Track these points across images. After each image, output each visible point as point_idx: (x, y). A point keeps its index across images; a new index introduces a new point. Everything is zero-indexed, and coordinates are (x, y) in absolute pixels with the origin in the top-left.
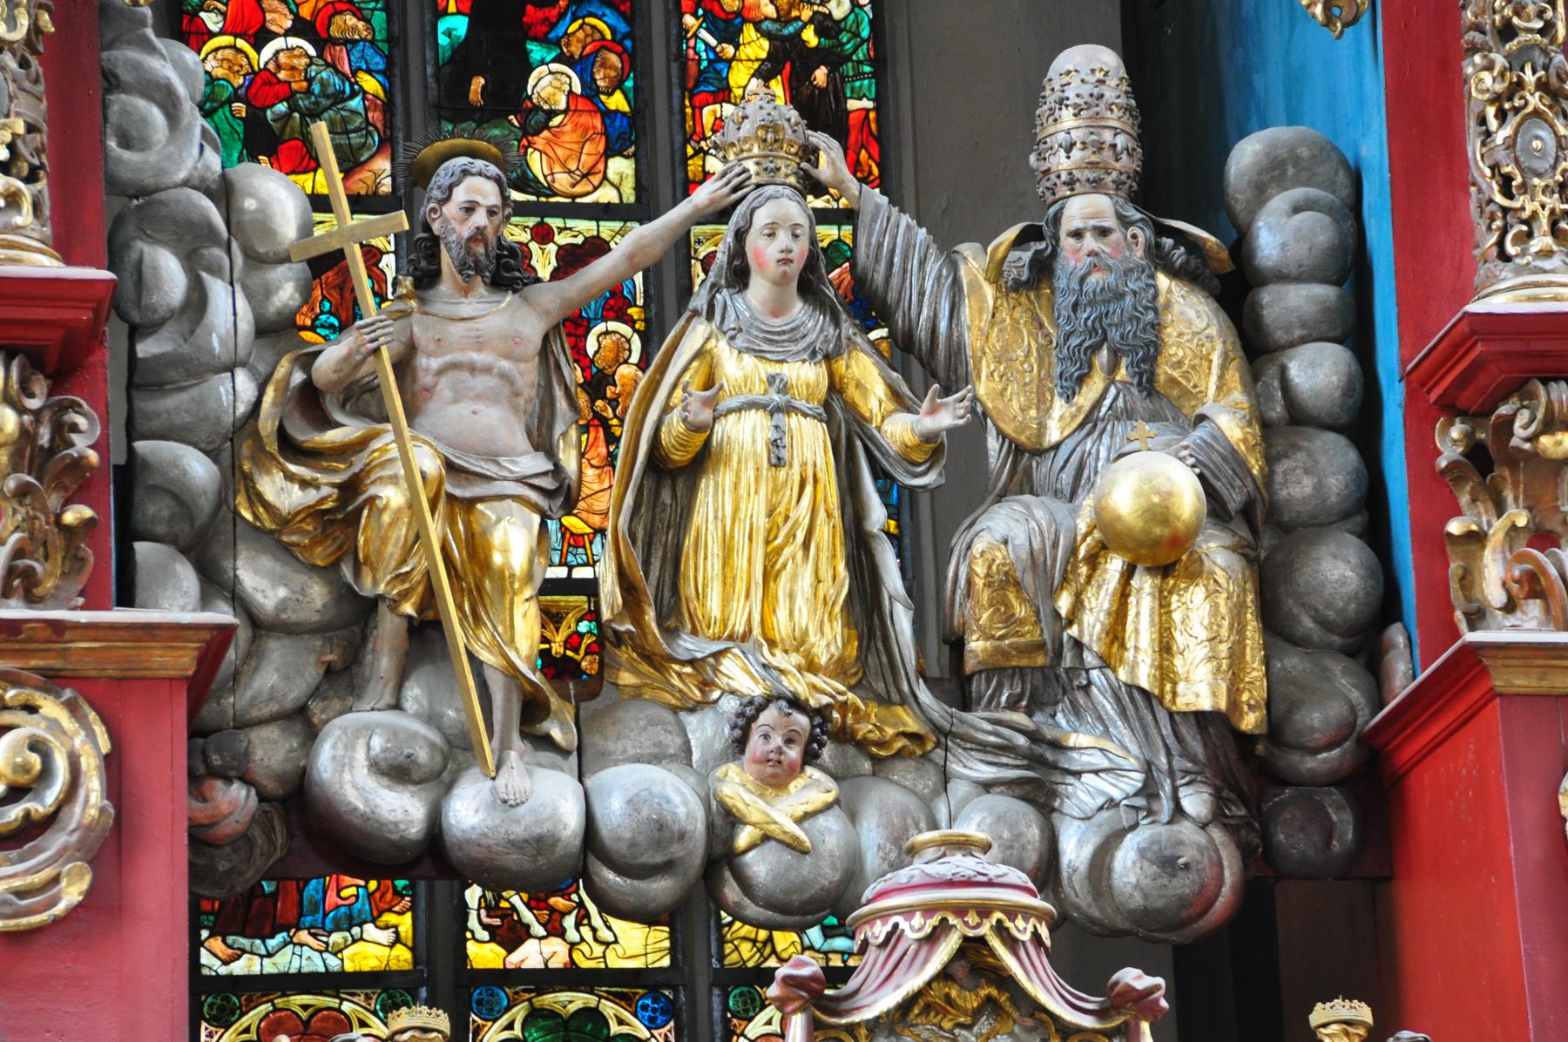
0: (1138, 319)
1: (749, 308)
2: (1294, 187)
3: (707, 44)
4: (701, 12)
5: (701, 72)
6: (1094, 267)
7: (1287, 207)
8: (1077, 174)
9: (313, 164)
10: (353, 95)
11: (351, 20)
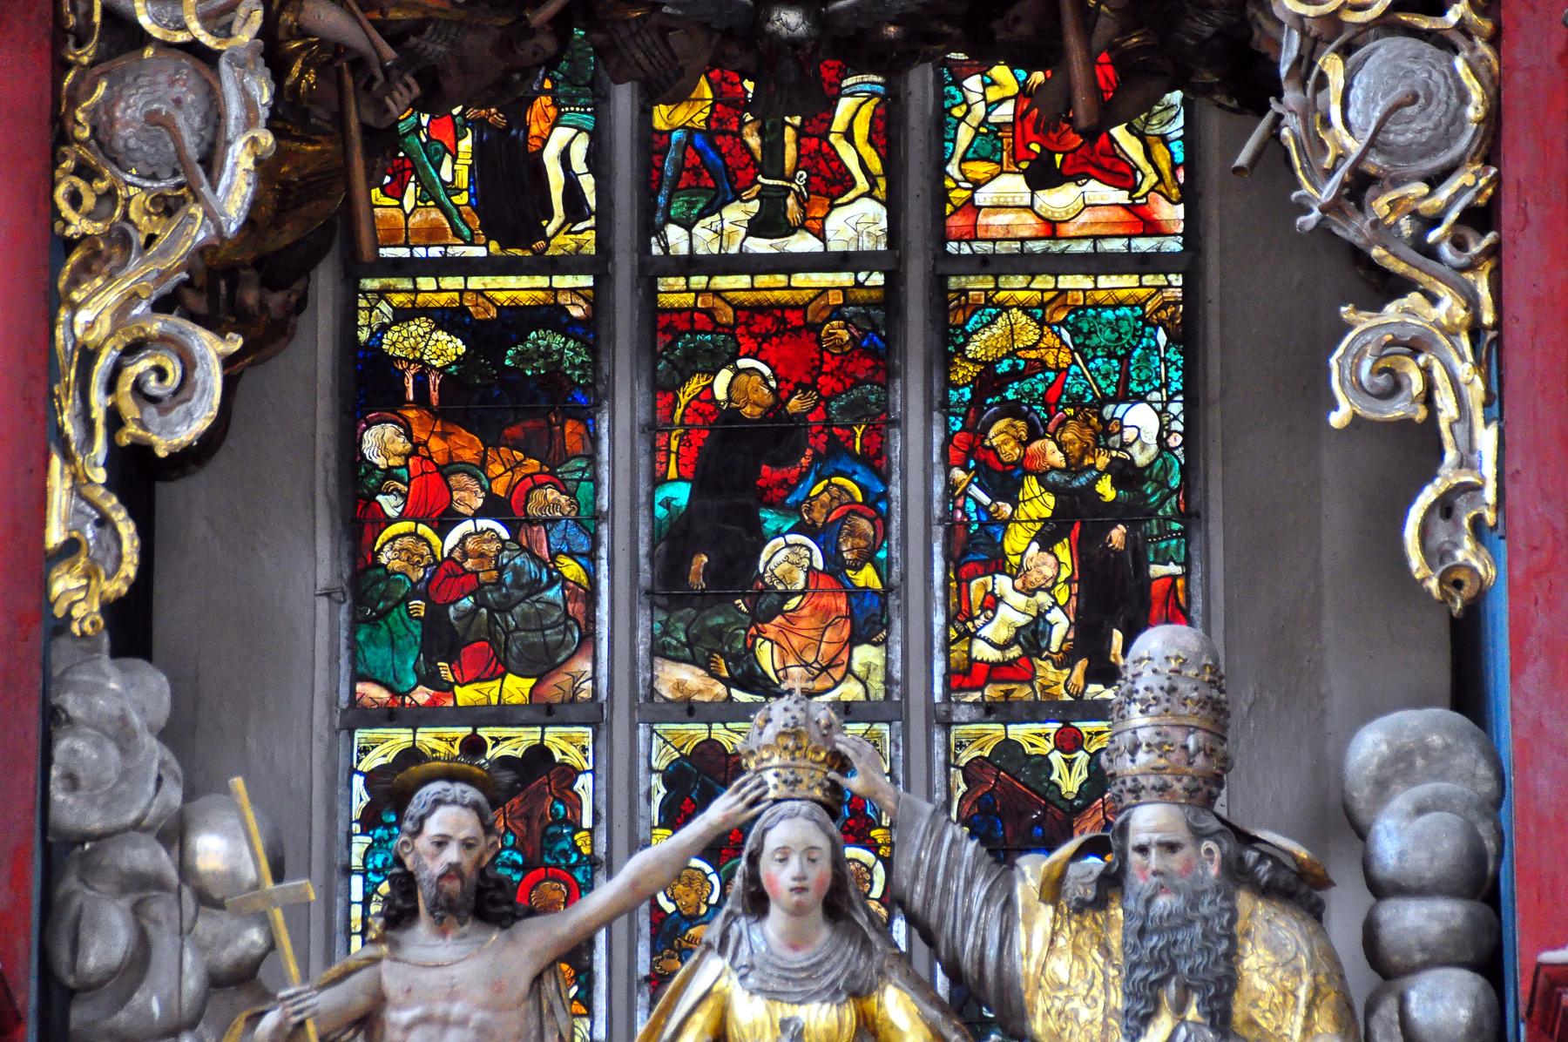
0: (1209, 950)
1: (765, 940)
2: (1424, 782)
3: (977, 502)
4: (972, 464)
5: (971, 537)
6: (1160, 889)
7: (1409, 807)
8: (1142, 781)
9: (501, 669)
10: (550, 586)
11: (552, 494)
